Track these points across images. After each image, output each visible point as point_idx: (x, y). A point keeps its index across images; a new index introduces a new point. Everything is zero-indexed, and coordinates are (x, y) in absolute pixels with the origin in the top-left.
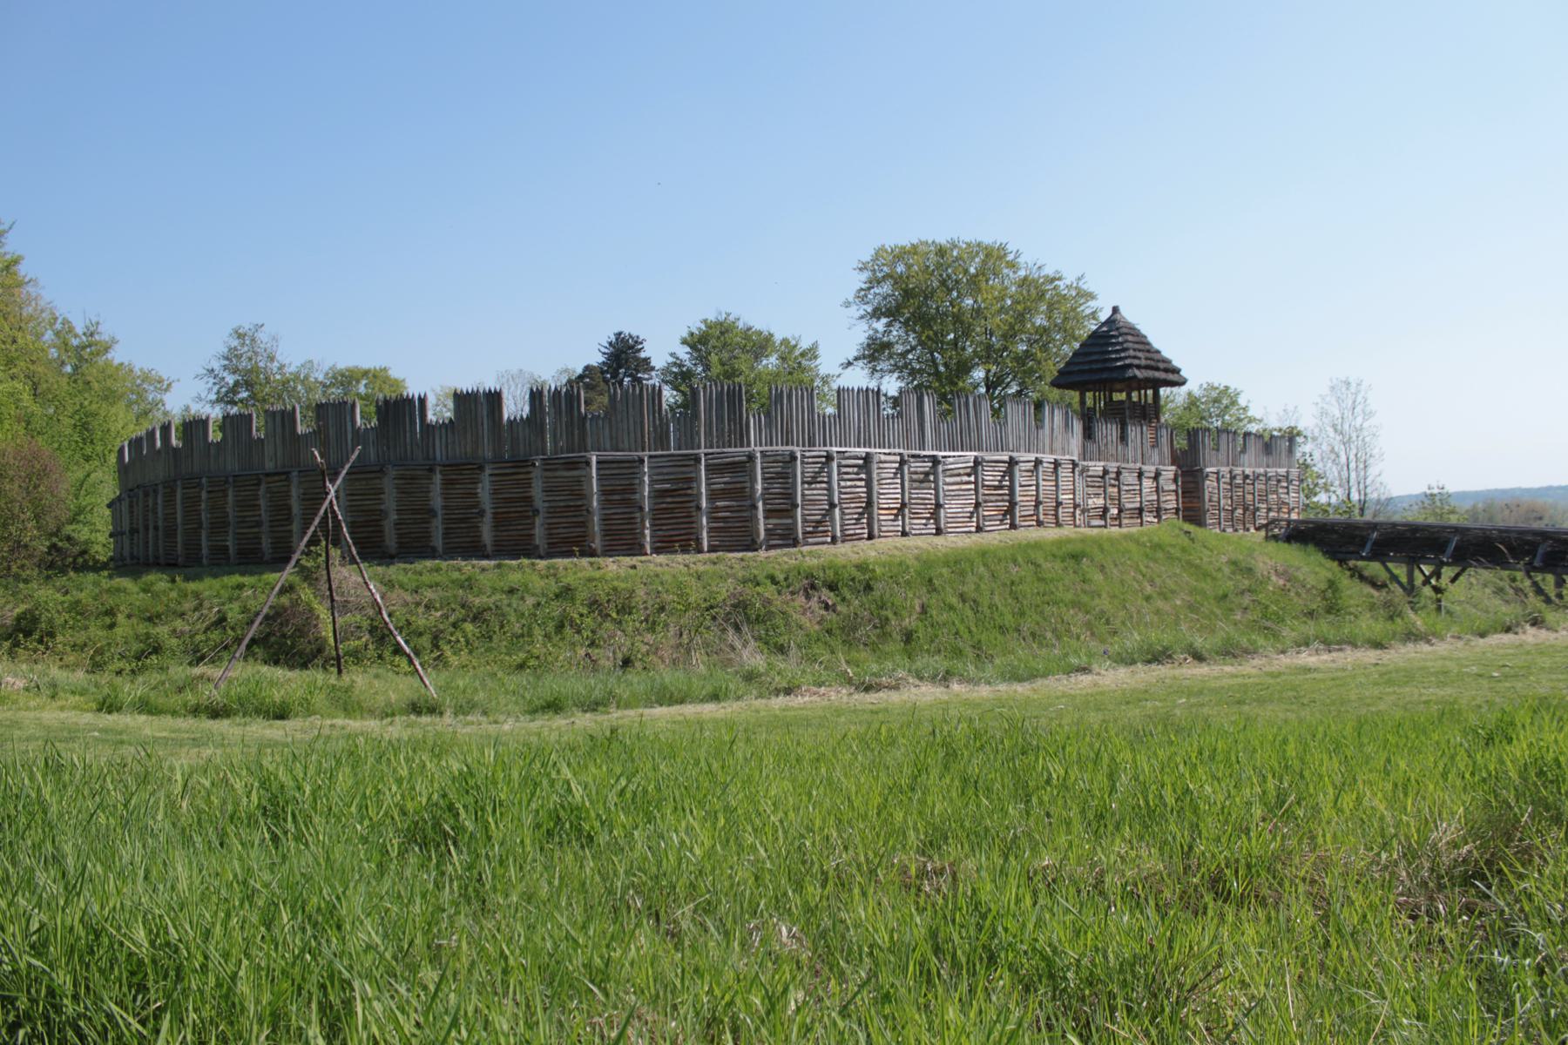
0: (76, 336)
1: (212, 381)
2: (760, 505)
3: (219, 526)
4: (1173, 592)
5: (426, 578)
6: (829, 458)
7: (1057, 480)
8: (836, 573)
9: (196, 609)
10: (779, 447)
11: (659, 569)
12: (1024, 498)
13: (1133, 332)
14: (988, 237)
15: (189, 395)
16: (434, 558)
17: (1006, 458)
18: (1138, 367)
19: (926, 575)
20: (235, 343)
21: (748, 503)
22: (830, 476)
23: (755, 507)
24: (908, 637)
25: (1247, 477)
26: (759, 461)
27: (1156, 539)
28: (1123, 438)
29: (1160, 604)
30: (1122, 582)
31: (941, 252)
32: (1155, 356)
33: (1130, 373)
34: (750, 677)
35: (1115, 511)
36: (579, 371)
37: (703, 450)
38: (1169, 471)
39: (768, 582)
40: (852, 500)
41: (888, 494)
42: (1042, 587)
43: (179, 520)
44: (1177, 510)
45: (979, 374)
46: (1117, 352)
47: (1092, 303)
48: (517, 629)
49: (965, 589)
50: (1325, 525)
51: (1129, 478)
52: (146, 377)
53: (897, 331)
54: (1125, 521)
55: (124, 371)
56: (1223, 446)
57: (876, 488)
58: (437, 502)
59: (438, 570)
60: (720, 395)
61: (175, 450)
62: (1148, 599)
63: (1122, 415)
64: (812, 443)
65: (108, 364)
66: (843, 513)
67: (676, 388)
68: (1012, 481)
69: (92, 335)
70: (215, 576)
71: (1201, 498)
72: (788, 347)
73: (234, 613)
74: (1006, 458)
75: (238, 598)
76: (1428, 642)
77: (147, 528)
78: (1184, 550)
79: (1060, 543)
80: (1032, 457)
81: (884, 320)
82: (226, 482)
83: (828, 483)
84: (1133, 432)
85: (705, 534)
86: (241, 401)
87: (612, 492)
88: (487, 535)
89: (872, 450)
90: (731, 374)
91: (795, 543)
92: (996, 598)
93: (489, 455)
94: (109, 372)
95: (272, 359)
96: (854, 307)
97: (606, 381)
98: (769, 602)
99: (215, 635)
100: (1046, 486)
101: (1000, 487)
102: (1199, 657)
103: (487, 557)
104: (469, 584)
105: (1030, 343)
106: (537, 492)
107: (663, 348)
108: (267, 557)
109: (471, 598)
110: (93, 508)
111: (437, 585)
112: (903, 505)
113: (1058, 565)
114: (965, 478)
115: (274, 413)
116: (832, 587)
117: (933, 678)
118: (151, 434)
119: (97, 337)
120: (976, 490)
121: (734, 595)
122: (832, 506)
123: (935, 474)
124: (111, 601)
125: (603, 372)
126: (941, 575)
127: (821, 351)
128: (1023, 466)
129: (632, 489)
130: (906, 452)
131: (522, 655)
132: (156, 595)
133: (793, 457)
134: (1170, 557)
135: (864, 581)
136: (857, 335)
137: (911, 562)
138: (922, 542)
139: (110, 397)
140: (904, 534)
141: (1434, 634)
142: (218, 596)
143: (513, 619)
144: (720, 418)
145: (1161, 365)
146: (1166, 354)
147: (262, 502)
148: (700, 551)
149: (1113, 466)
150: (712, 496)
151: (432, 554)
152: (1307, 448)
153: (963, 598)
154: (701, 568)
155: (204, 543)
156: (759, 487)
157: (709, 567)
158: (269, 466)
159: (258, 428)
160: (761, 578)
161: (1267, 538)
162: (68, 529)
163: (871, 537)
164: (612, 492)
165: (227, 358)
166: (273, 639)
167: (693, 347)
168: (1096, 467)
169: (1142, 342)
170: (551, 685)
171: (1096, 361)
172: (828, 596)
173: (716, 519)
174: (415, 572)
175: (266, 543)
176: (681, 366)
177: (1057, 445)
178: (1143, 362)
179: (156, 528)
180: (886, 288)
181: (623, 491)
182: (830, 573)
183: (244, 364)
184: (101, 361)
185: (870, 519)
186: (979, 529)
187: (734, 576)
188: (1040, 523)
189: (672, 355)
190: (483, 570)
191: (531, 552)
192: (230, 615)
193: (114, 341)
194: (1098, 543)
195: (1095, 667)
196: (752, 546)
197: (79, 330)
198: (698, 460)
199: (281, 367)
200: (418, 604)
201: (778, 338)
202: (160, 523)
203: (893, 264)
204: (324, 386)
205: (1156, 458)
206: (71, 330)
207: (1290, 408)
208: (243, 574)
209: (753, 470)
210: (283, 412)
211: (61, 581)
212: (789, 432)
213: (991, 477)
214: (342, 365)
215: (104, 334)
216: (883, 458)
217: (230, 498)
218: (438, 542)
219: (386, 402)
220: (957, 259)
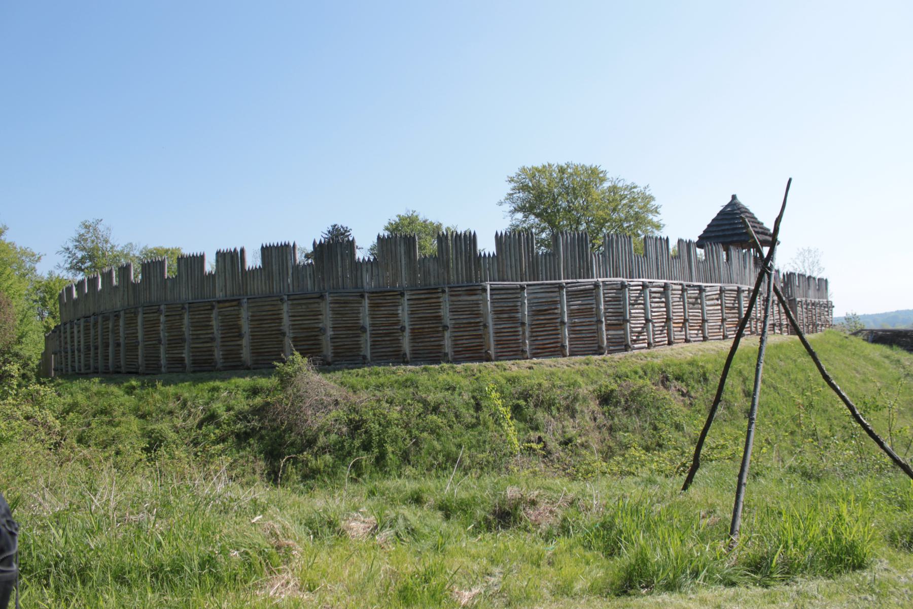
1: (67, 255)
3: (177, 341)
15: (53, 262)
17: (736, 288)
20: (83, 231)
22: (645, 300)
43: (140, 338)
52: (24, 252)
58: (366, 321)
61: (135, 285)
66: (654, 326)
74: (736, 288)
77: (107, 346)
82: (183, 308)
87: (502, 312)
88: (406, 345)
93: (405, 283)
95: (107, 242)
101: (733, 308)
106: (445, 312)
108: (111, 369)
112: (686, 320)
114: (716, 302)
120: (722, 309)
124: (103, 403)
140: (687, 341)
147: (214, 323)
150: (572, 314)
151: (362, 362)
155: (162, 355)
158: (220, 295)
162: (16, 348)
163: (670, 343)
164: (502, 312)
171: (728, 230)
175: (218, 354)
181: (510, 311)
185: (669, 330)
199: (112, 247)
202: (122, 341)
209: (598, 295)
217: (186, 321)
218: (367, 352)
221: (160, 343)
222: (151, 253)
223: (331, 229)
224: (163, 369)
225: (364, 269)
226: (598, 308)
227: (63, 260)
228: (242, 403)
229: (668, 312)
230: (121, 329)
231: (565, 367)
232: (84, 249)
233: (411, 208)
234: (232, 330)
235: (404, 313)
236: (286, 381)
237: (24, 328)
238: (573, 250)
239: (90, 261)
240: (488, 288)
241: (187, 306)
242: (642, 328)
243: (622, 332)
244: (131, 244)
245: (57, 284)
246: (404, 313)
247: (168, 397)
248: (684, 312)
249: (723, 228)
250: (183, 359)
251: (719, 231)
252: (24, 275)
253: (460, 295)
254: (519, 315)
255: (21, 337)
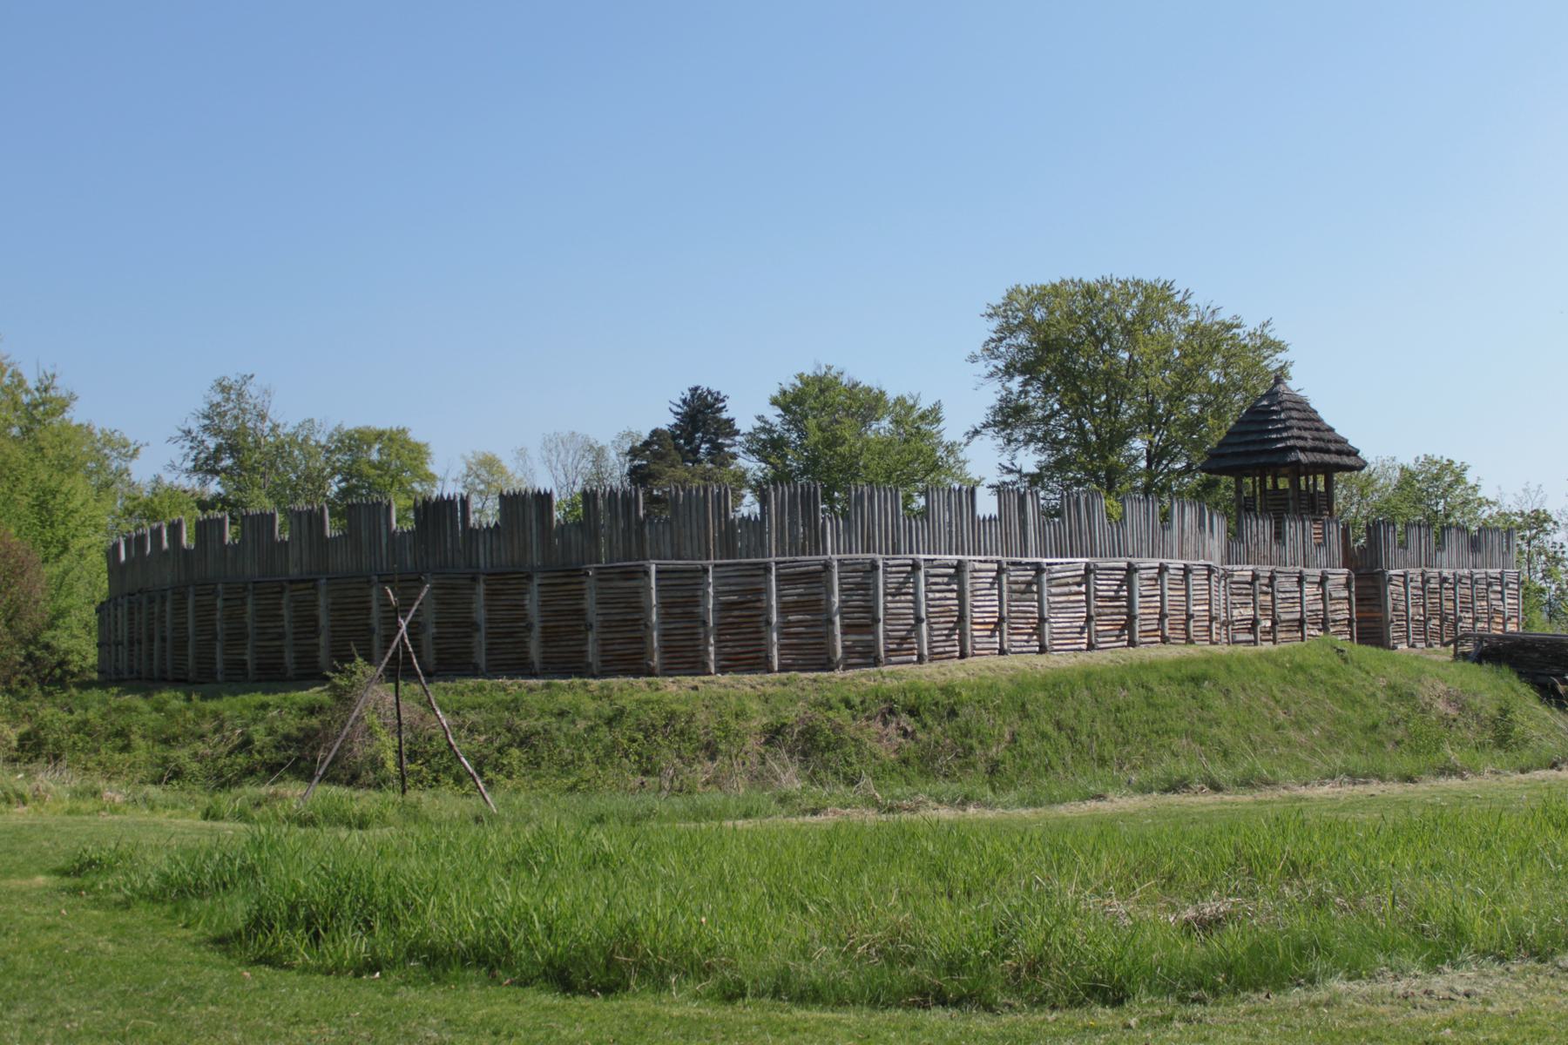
0: (27, 392)
1: (188, 444)
2: (837, 619)
4: (1310, 721)
5: (468, 699)
6: (915, 566)
7: (1187, 589)
8: (918, 697)
9: (216, 731)
10: (860, 555)
11: (722, 690)
12: (1145, 612)
13: (1302, 406)
14: (1149, 273)
15: (157, 454)
16: (476, 676)
17: (1124, 565)
18: (1303, 449)
19: (1019, 700)
20: (218, 398)
21: (823, 617)
22: (916, 587)
23: (831, 622)
24: (994, 768)
25: (1445, 580)
26: (836, 570)
27: (1298, 659)
28: (1279, 535)
29: (1292, 734)
30: (1250, 709)
31: (1089, 292)
32: (1326, 435)
33: (1292, 457)
34: (783, 800)
35: (1269, 624)
36: (646, 435)
37: (774, 559)
38: (1339, 575)
39: (842, 707)
40: (941, 614)
41: (984, 607)
42: (1151, 714)
43: (191, 630)
44: (1350, 621)
45: (1138, 445)
46: (1278, 431)
47: (1281, 356)
48: (567, 755)
49: (1063, 716)
50: (1524, 641)
51: (1286, 584)
52: (108, 441)
53: (1034, 395)
54: (1280, 635)
55: (85, 431)
56: (1413, 543)
57: (969, 600)
58: (480, 614)
59: (481, 689)
60: (793, 497)
61: (187, 552)
62: (1277, 728)
63: (1278, 508)
64: (896, 551)
65: (65, 426)
66: (931, 629)
67: (764, 459)
68: (1130, 591)
69: (46, 390)
70: (235, 694)
71: (1382, 605)
72: (903, 411)
73: (260, 736)
75: (263, 719)
76: (1462, 777)
77: (151, 639)
78: (1332, 672)
79: (1178, 663)
80: (1156, 562)
81: (1019, 379)
82: (245, 589)
83: (915, 594)
84: (1292, 528)
85: (775, 652)
86: (224, 470)
87: (673, 605)
88: (535, 650)
89: (966, 558)
90: (832, 442)
91: (876, 662)
92: (1098, 726)
93: (537, 562)
94: (65, 436)
95: (262, 417)
96: (982, 363)
97: (678, 448)
98: (841, 727)
99: (241, 759)
100: (1174, 596)
101: (1117, 598)
102: (1216, 788)
103: (535, 676)
104: (515, 706)
105: (1204, 404)
106: (590, 603)
107: (749, 409)
108: (290, 673)
109: (517, 721)
110: (74, 605)
111: (480, 706)
112: (1001, 619)
113: (1174, 688)
114: (1075, 588)
115: (299, 514)
116: (913, 712)
117: (952, 803)
118: (156, 534)
119: (52, 393)
120: (1088, 601)
121: (802, 720)
122: (919, 620)
123: (1039, 584)
124: (121, 721)
125: (674, 437)
126: (1037, 700)
127: (945, 413)
128: (1145, 574)
129: (695, 601)
130: (1004, 559)
131: (573, 779)
132: (170, 716)
133: (875, 567)
134: (1313, 681)
135: (948, 705)
136: (990, 395)
137: (1004, 684)
138: (1025, 662)
139: (66, 466)
140: (1002, 652)
141: (1470, 770)
142: (241, 716)
143: (563, 744)
144: (793, 523)
145: (1333, 447)
146: (1341, 431)
147: (285, 612)
148: (770, 671)
149: (1264, 570)
150: (784, 609)
151: (474, 672)
152: (1559, 537)
153: (1059, 726)
154: (769, 690)
155: (219, 657)
156: (836, 599)
157: (778, 689)
158: (294, 572)
159: (282, 533)
160: (833, 701)
161: (1456, 656)
162: (47, 636)
163: (963, 656)
164: (673, 605)
165: (206, 417)
166: (302, 764)
167: (786, 409)
168: (1244, 572)
169: (1310, 418)
170: (598, 803)
171: (1254, 442)
172: (906, 721)
173: (788, 635)
174: (456, 692)
175: (289, 658)
176: (770, 431)
177: (1189, 548)
178: (1310, 443)
179: (163, 639)
180: (1022, 339)
181: (686, 604)
182: (912, 697)
183: (229, 425)
184: (56, 422)
186: (1091, 647)
187: (805, 699)
188: (1165, 640)
189: (760, 418)
190: (531, 690)
191: (583, 671)
192: (256, 737)
193: (73, 397)
194: (1226, 664)
195: (1111, 795)
196: (828, 665)
197: (31, 383)
198: (767, 569)
199: (275, 428)
200: (460, 727)
201: (891, 395)
202: (168, 634)
203: (1029, 309)
204: (328, 451)
205: (1322, 557)
206: (21, 383)
207: (1533, 487)
208: (266, 692)
210: (310, 512)
211: (61, 698)
212: (871, 537)
213: (1105, 586)
214: (350, 425)
215: (61, 389)
216: (978, 566)
217: (249, 608)
218: (481, 658)
219: (426, 503)
220: (1110, 302)
221: (215, 638)
222: (351, 438)
223: (688, 395)
224: (219, 677)
225: (481, 541)
226: (829, 600)
227: (180, 455)
228: (290, 724)
229: (962, 606)
230: (168, 617)
231: (748, 689)
232: (218, 432)
233: (825, 361)
234: (307, 623)
235: (532, 603)
236: (344, 698)
237: (63, 603)
238: (792, 513)
239: (232, 456)
240: (653, 568)
241: (250, 586)
242: (993, 631)
243: (870, 637)
244: (311, 421)
245: (166, 503)
246: (532, 603)
247: (204, 716)
248: (1001, 606)
249: (1250, 438)
250: (244, 663)
251: (1240, 444)
252: (107, 485)
253: (611, 580)
254: (701, 610)
255: (55, 618)
